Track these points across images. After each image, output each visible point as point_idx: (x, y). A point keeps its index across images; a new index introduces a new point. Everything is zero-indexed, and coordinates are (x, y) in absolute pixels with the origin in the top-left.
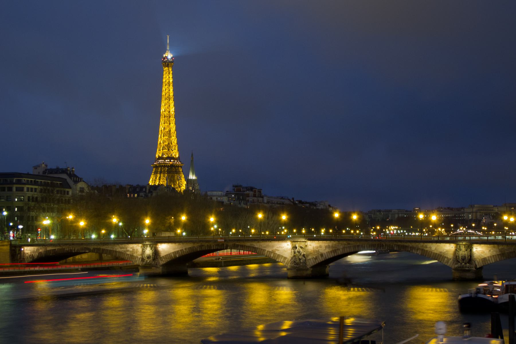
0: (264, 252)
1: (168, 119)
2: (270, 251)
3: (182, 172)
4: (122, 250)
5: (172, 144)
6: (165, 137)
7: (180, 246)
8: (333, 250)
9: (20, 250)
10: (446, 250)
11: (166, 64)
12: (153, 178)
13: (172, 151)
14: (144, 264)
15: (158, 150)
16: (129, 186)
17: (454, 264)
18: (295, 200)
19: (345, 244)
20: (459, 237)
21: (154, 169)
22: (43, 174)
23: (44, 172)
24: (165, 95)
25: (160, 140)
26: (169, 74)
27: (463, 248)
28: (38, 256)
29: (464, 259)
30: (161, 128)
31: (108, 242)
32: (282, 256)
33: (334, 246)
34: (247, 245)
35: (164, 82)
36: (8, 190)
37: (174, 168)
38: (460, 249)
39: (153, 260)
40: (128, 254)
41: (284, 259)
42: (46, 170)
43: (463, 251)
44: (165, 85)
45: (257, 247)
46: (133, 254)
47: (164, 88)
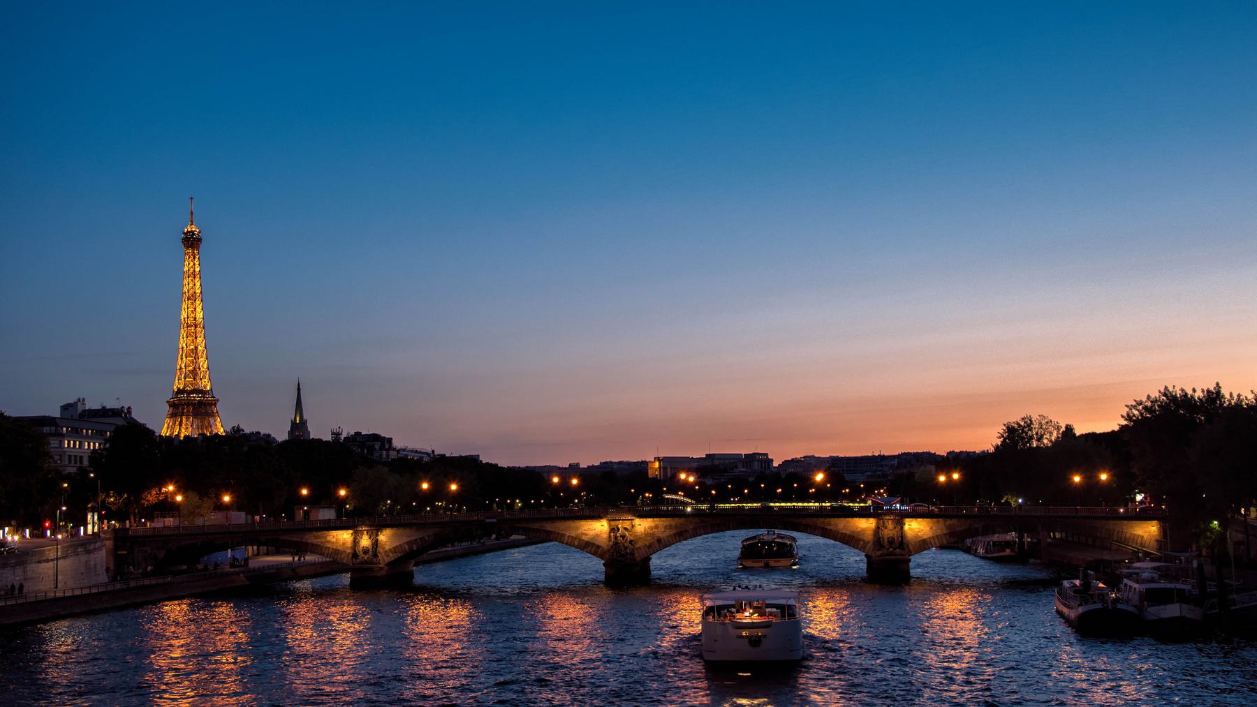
5: (200, 369)
26: (194, 259)
27: (890, 525)
29: (891, 541)
45: (550, 530)
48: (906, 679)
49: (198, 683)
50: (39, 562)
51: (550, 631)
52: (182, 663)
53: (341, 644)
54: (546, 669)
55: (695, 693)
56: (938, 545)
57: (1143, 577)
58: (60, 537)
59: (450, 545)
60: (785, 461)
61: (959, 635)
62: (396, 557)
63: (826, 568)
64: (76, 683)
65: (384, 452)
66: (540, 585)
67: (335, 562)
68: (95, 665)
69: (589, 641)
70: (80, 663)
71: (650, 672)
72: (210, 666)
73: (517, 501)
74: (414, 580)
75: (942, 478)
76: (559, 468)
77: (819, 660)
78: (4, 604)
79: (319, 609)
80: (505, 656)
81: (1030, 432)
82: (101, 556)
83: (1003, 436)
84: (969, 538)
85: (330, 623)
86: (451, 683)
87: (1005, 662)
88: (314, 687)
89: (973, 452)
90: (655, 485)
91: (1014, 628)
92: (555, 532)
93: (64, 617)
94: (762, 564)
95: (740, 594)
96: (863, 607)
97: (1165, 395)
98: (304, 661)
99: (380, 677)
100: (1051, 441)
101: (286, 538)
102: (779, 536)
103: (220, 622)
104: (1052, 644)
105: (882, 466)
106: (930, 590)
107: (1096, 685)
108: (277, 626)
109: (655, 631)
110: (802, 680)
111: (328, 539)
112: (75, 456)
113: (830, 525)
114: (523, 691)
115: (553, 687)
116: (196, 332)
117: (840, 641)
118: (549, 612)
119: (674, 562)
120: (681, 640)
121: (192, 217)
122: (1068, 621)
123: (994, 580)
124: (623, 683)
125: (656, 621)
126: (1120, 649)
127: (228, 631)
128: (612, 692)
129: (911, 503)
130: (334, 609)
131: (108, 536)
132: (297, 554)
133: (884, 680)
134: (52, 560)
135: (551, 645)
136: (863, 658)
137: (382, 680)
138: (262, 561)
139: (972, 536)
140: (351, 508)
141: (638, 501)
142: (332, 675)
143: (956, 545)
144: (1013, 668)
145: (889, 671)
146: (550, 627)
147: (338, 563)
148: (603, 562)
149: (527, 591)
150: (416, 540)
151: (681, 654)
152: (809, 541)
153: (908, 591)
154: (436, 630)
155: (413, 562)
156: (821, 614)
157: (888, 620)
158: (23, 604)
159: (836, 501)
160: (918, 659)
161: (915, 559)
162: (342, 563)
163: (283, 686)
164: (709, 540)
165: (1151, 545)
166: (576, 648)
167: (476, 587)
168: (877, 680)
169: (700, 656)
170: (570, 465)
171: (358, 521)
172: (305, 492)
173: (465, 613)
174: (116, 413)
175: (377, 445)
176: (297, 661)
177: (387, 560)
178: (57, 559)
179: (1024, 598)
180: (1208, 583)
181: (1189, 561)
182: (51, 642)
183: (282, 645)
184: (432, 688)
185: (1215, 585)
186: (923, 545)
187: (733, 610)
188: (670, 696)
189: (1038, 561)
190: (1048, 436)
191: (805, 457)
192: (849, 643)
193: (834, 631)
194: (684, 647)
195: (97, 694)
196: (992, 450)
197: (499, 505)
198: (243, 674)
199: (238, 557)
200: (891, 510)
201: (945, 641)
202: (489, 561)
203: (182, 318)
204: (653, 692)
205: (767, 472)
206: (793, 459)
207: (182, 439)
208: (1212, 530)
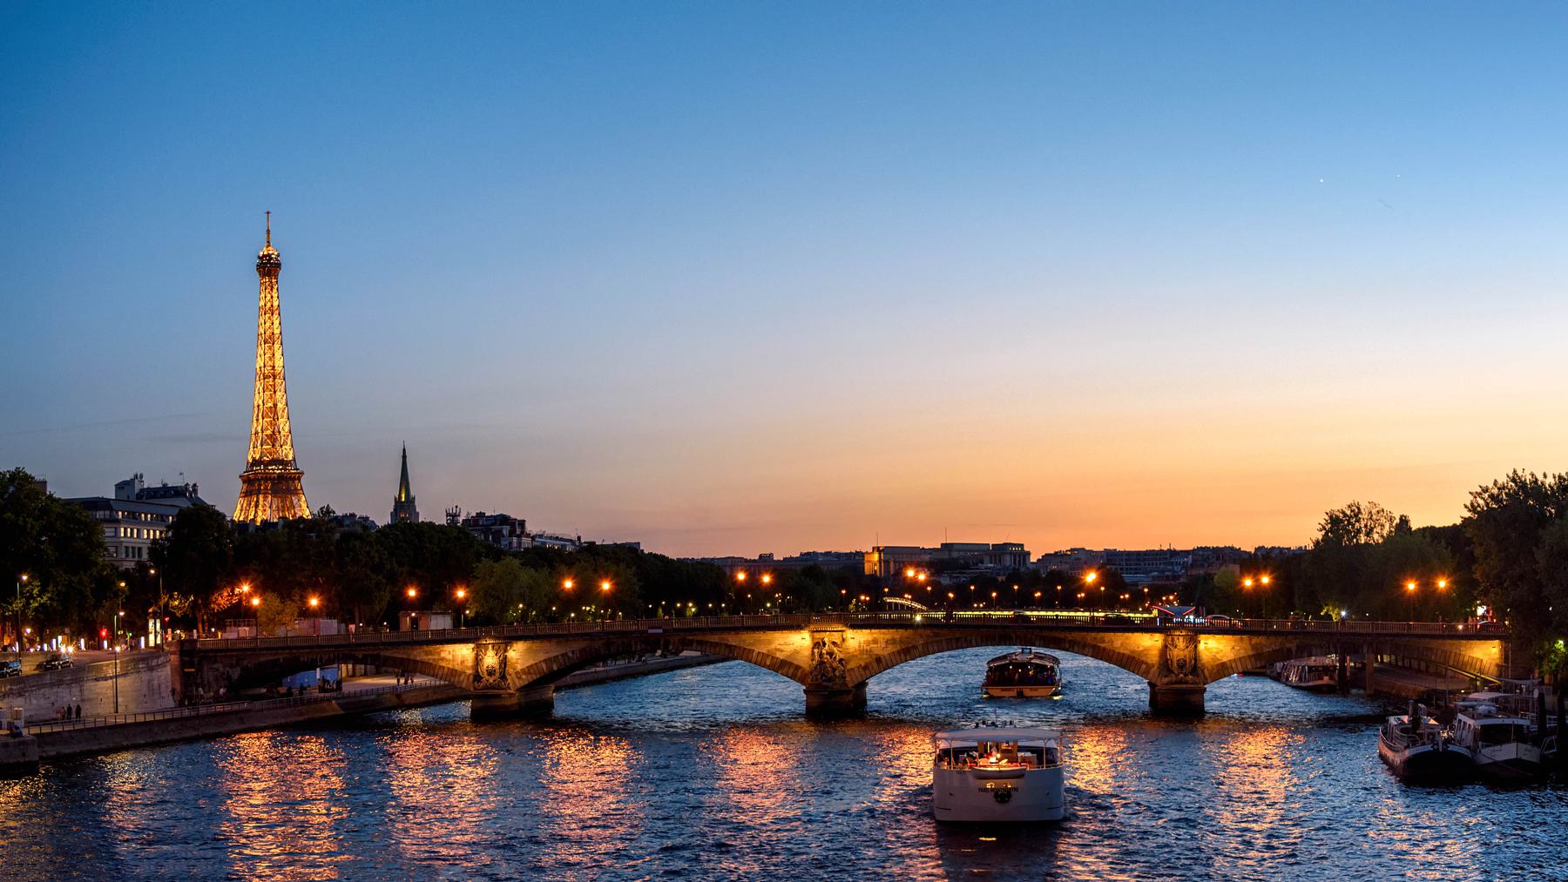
4: (430, 657)
5: (280, 432)
15: (251, 446)
19: (928, 636)
26: (272, 290)
27: (1181, 643)
45: (733, 644)
48: (1193, 844)
49: (284, 838)
50: (97, 680)
51: (733, 779)
52: (265, 812)
53: (461, 794)
54: (728, 830)
55: (923, 863)
56: (1241, 670)
57: (1479, 712)
58: (118, 649)
59: (601, 664)
60: (1046, 555)
61: (1261, 788)
62: (531, 680)
63: (1097, 699)
64: (144, 829)
65: (515, 540)
66: (721, 718)
67: (452, 686)
68: (163, 810)
69: (784, 794)
70: (147, 805)
71: (865, 835)
72: (298, 817)
73: (690, 605)
74: (554, 711)
75: (1248, 583)
76: (746, 561)
77: (1084, 821)
78: (61, 730)
79: (431, 748)
80: (673, 813)
81: (1357, 524)
82: (165, 674)
83: (1324, 528)
84: (1279, 661)
85: (446, 766)
86: (603, 847)
87: (1315, 821)
88: (427, 849)
89: (1287, 549)
90: (874, 585)
91: (1329, 778)
92: (740, 648)
93: (126, 749)
94: (1014, 693)
95: (985, 733)
96: (1143, 752)
97: (1514, 480)
98: (415, 814)
99: (511, 838)
100: (1382, 536)
101: (388, 653)
102: (1037, 656)
103: (309, 762)
104: (1372, 797)
105: (1172, 564)
106: (1229, 730)
107: (1418, 846)
108: (379, 769)
109: (872, 781)
110: (1062, 847)
111: (443, 655)
112: (133, 548)
113: (1104, 642)
114: (697, 859)
115: (739, 855)
116: (274, 385)
117: (1112, 796)
118: (731, 755)
119: (899, 689)
120: (906, 793)
121: (268, 236)
122: (1391, 767)
123: (1308, 717)
124: (829, 850)
125: (873, 767)
126: (1448, 800)
127: (318, 773)
128: (815, 862)
129: (1208, 614)
130: (450, 747)
131: (173, 649)
132: (403, 676)
133: (1167, 846)
134: (111, 678)
135: (735, 798)
136: (1141, 818)
137: (513, 842)
138: (358, 684)
139: (1283, 660)
140: (472, 615)
141: (851, 606)
142: (449, 835)
143: (1262, 670)
144: (1324, 828)
145: (1173, 833)
146: (734, 774)
147: (455, 688)
148: (804, 688)
149: (703, 726)
150: (557, 656)
151: (905, 812)
152: (1076, 663)
153: (1201, 730)
154: (584, 778)
155: (553, 686)
156: (1089, 760)
157: (1174, 768)
158: (81, 731)
159: (1112, 610)
160: (1210, 818)
161: (1212, 689)
162: (461, 688)
163: (389, 846)
164: (945, 659)
165: (1491, 671)
166: (767, 803)
167: (635, 721)
168: (1158, 847)
169: (930, 815)
170: (760, 556)
171: (481, 632)
172: (412, 593)
173: (621, 755)
174: (179, 492)
175: (506, 530)
176: (404, 814)
177: (519, 683)
178: (116, 677)
179: (1342, 740)
180: (1548, 717)
181: (1530, 692)
182: (113, 777)
183: (384, 796)
184: (579, 854)
185: (1554, 719)
186: (1222, 670)
187: (975, 754)
188: (891, 867)
189: (1362, 692)
190: (1378, 529)
191: (1072, 550)
192: (1124, 798)
193: (1105, 782)
194: (910, 802)
195: (168, 844)
196: (1311, 546)
197: (667, 610)
198: (338, 829)
199: (328, 678)
200: (1182, 623)
201: (1244, 795)
202: (652, 686)
203: (258, 367)
204: (868, 862)
205: (1022, 569)
206: (1056, 553)
207: (258, 524)
208: (1555, 652)
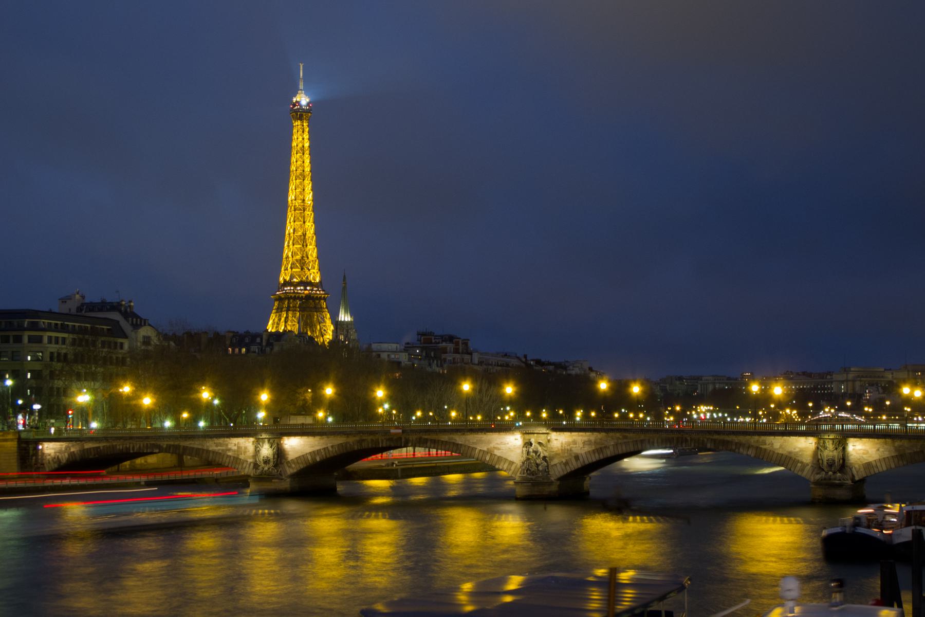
0: (473, 453)
1: (301, 213)
2: (484, 451)
3: (327, 308)
4: (219, 448)
5: (308, 258)
6: (295, 246)
7: (322, 441)
8: (597, 449)
9: (36, 449)
10: (799, 448)
11: (297, 115)
12: (274, 320)
13: (309, 270)
14: (257, 473)
15: (283, 269)
16: (231, 334)
17: (814, 473)
18: (528, 359)
19: (618, 438)
20: (822, 425)
21: (276, 304)
22: (77, 312)
23: (79, 309)
24: (296, 170)
25: (287, 252)
26: (303, 132)
27: (830, 445)
28: (68, 459)
29: (831, 464)
30: (288, 229)
31: (193, 434)
32: (506, 460)
33: (598, 441)
34: (442, 440)
35: (294, 146)
36: (15, 342)
37: (311, 301)
38: (824, 447)
39: (274, 467)
40: (230, 456)
41: (509, 464)
42: (83, 305)
43: (829, 450)
44: (295, 152)
45: (460, 443)
46: (238, 455)
47: (293, 158)
